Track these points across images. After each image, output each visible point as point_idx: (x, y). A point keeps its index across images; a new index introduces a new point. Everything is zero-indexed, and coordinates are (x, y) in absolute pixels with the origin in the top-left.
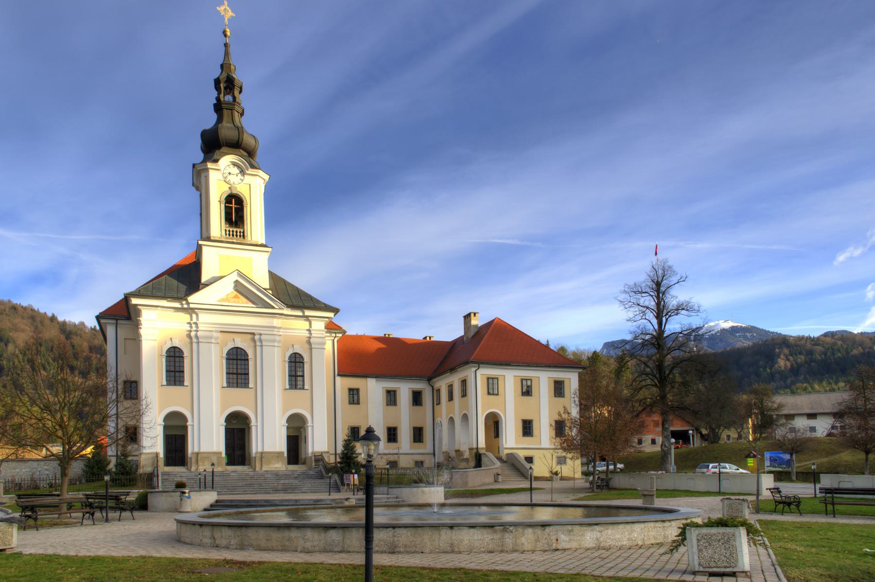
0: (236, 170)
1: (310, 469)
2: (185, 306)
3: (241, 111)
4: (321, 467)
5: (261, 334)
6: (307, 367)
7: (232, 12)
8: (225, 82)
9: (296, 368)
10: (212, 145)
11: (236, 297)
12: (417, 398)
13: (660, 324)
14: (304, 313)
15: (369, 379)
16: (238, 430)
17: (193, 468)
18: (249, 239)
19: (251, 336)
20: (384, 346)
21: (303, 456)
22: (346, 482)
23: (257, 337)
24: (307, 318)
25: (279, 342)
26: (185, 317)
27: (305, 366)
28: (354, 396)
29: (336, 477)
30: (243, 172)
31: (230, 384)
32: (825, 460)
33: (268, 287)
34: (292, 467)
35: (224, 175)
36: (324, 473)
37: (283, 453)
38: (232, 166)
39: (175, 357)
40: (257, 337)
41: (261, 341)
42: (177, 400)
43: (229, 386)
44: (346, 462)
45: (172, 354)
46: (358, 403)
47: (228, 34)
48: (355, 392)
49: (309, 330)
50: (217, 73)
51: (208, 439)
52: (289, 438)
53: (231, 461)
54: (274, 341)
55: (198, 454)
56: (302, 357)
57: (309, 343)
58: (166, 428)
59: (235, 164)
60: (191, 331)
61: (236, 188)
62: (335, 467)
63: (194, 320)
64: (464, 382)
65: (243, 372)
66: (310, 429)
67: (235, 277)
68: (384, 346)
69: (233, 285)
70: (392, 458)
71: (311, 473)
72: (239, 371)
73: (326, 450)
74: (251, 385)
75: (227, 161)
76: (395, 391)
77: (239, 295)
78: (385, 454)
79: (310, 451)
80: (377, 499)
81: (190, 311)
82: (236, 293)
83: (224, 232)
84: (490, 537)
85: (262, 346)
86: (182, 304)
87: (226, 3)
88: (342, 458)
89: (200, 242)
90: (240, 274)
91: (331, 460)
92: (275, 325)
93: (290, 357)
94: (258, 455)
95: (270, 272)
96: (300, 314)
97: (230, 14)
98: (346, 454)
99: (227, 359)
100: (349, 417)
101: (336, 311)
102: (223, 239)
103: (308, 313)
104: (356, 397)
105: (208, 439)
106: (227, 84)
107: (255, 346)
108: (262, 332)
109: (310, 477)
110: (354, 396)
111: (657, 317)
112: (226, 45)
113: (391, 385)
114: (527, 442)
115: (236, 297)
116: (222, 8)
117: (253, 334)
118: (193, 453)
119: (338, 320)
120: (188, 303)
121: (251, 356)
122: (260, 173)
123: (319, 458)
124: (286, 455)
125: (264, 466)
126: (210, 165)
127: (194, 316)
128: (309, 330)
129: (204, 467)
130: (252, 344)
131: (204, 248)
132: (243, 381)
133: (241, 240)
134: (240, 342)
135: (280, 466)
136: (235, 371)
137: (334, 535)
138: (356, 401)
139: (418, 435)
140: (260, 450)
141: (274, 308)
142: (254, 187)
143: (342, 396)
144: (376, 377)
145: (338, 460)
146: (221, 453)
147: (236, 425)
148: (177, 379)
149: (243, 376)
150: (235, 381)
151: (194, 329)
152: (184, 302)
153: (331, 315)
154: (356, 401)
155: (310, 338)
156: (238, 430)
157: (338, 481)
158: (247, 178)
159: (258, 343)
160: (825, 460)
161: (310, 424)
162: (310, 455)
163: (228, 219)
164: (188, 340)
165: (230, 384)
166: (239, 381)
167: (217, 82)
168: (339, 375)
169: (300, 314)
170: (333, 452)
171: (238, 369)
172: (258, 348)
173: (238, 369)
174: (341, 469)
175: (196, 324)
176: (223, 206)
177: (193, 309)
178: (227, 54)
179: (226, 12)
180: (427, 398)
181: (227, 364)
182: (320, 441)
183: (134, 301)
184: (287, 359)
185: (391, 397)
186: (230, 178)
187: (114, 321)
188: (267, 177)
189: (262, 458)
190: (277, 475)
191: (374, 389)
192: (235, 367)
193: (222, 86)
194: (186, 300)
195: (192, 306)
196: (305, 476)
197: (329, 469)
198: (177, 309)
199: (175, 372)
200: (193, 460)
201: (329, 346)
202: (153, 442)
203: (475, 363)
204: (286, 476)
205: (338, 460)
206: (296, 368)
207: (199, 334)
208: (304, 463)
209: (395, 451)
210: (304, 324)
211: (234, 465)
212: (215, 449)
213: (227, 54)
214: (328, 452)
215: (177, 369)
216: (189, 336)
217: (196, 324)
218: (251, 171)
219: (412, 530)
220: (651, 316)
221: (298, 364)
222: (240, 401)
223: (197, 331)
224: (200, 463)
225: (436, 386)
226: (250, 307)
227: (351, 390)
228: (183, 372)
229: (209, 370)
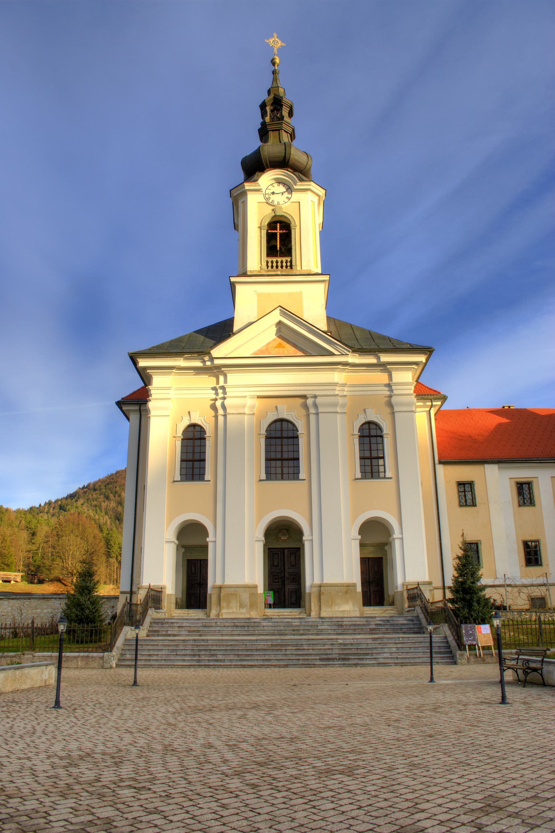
0: (282, 189)
1: (401, 613)
2: (208, 363)
3: (290, 130)
4: (418, 610)
5: (315, 397)
6: (388, 442)
7: (282, 42)
8: (272, 105)
9: (371, 448)
10: (254, 167)
11: (279, 346)
14: (378, 358)
15: (487, 466)
16: (284, 552)
17: (213, 613)
18: (298, 268)
19: (301, 401)
20: (505, 420)
21: (390, 591)
22: (467, 641)
23: (310, 401)
24: (383, 367)
25: (343, 406)
26: (208, 381)
27: (385, 440)
28: (466, 493)
29: (445, 630)
30: (290, 189)
31: (270, 475)
34: (371, 611)
35: (266, 196)
36: (424, 621)
37: (354, 585)
38: (275, 185)
39: (370, 436)
40: (310, 401)
41: (315, 406)
42: (194, 503)
44: (463, 599)
46: (474, 505)
47: (277, 61)
48: (467, 488)
49: (389, 386)
50: (264, 96)
51: (240, 566)
52: (364, 561)
53: (280, 602)
54: (336, 405)
55: (220, 588)
56: (380, 429)
57: (390, 405)
59: (279, 182)
60: (216, 400)
61: (281, 208)
62: (444, 610)
63: (221, 383)
65: (291, 456)
66: (397, 544)
67: (276, 317)
68: (505, 420)
69: (274, 329)
70: (537, 592)
71: (402, 621)
72: (285, 456)
73: (427, 579)
74: (302, 475)
75: (267, 179)
76: (529, 484)
77: (284, 343)
78: (525, 586)
79: (400, 581)
80: (504, 653)
81: (216, 371)
82: (280, 340)
83: (264, 264)
85: (317, 414)
86: (204, 362)
88: (455, 590)
89: (233, 279)
90: (285, 312)
91: (435, 597)
92: (336, 381)
93: (361, 429)
94: (315, 590)
96: (373, 361)
97: (280, 44)
98: (463, 583)
99: (267, 438)
100: (460, 525)
102: (263, 273)
103: (385, 358)
104: (469, 496)
107: (308, 415)
108: (317, 393)
109: (397, 629)
110: (466, 493)
112: (274, 72)
113: (523, 473)
115: (279, 346)
116: (271, 40)
117: (305, 397)
118: (214, 587)
120: (212, 359)
121: (301, 430)
122: (313, 186)
123: (415, 595)
124: (359, 589)
125: (323, 609)
126: (248, 186)
127: (221, 378)
128: (389, 386)
129: (231, 611)
130: (304, 412)
131: (238, 288)
132: (291, 470)
133: (288, 271)
134: (287, 411)
135: (351, 608)
136: (279, 456)
138: (469, 501)
140: (317, 581)
141: (332, 354)
142: (307, 209)
143: (448, 495)
144: (498, 462)
145: (449, 595)
146: (256, 587)
147: (284, 542)
148: (196, 471)
149: (291, 463)
150: (279, 470)
151: (221, 395)
152: (206, 358)
154: (469, 501)
155: (390, 396)
156: (284, 552)
157: (451, 639)
158: (296, 196)
159: (312, 411)
161: (396, 534)
162: (400, 589)
163: (271, 251)
164: (213, 413)
165: (270, 475)
166: (285, 470)
167: (263, 106)
168: (440, 463)
169: (373, 361)
170: (440, 584)
172: (313, 418)
173: (282, 448)
174: (456, 612)
175: (223, 388)
176: (264, 232)
177: (219, 367)
178: (275, 80)
179: (275, 43)
181: (268, 446)
182: (416, 566)
184: (356, 432)
186: (273, 197)
187: (137, 408)
188: (321, 192)
189: (320, 594)
190: (340, 626)
191: (496, 482)
192: (279, 448)
193: (268, 109)
194: (209, 353)
195: (217, 362)
196: (390, 626)
197: (434, 616)
198: (198, 370)
199: (193, 461)
200: (214, 599)
201: (421, 423)
204: (355, 628)
205: (449, 595)
206: (371, 448)
207: (227, 402)
208: (392, 604)
209: (541, 581)
210: (381, 377)
211: (284, 606)
212: (247, 581)
213: (275, 80)
214: (430, 583)
215: (197, 457)
216: (214, 407)
217: (223, 388)
218: (300, 185)
221: (373, 440)
222: (286, 502)
223: (224, 398)
224: (223, 604)
226: (300, 354)
228: (204, 460)
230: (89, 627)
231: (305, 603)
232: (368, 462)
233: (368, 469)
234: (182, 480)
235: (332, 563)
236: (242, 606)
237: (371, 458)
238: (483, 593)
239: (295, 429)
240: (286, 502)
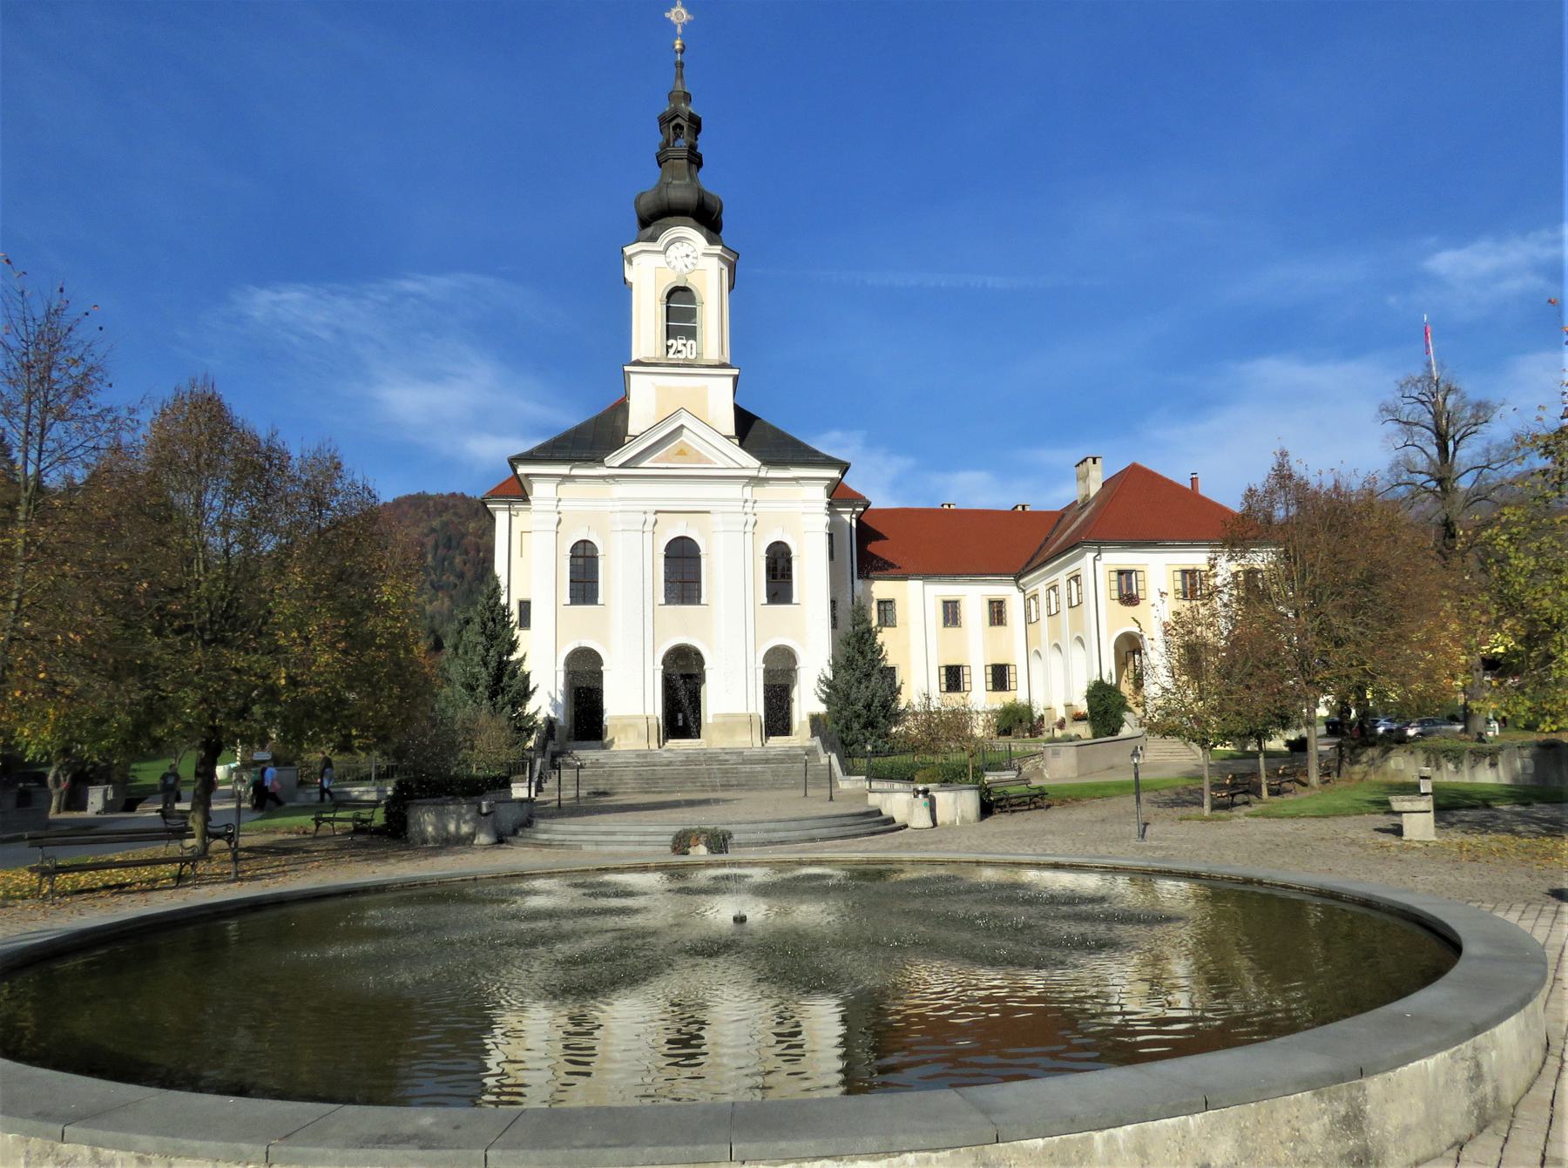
12: (997, 612)
16: (683, 679)
32: (992, 980)
45: (580, 552)
51: (631, 699)
58: (767, 672)
84: (550, 1014)
87: (679, 3)
89: (627, 368)
95: (737, 408)
101: (844, 468)
105: (631, 699)
113: (950, 590)
114: (954, 700)
119: (853, 482)
153: (835, 474)
156: (683, 679)
160: (992, 980)
171: (683, 570)
173: (683, 570)
179: (678, 15)
183: (522, 470)
185: (951, 612)
202: (546, 698)
203: (1093, 544)
222: (682, 625)
229: (632, 571)
239: (594, 548)
240: (682, 625)
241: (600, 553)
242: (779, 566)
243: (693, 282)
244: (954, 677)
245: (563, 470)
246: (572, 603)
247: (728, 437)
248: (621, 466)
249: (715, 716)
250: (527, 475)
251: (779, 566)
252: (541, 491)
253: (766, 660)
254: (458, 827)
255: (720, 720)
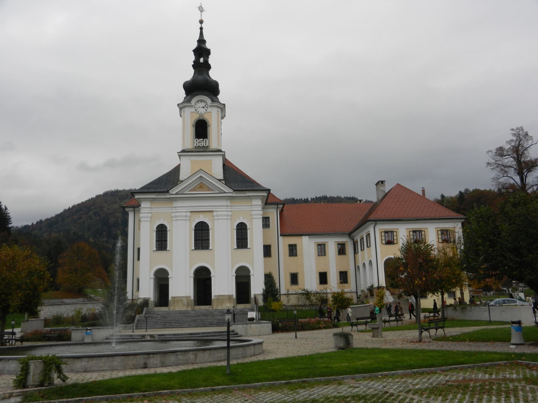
12: (342, 250)
13: (522, 179)
15: (303, 237)
16: (202, 279)
33: (222, 178)
39: (242, 229)
43: (196, 249)
45: (160, 229)
50: (195, 45)
51: (182, 287)
64: (368, 235)
76: (324, 245)
106: (202, 51)
111: (519, 174)
113: (321, 240)
137: (191, 356)
139: (343, 277)
144: (309, 235)
148: (163, 246)
149: (198, 238)
156: (202, 279)
166: (203, 245)
168: (281, 235)
171: (202, 236)
173: (202, 236)
180: (349, 248)
185: (322, 250)
202: (147, 291)
219: (123, 358)
220: (512, 172)
222: (202, 259)
225: (355, 239)
227: (290, 246)
229: (181, 236)
230: (369, 295)
231: (116, 379)
232: (240, 241)
233: (240, 244)
234: (156, 250)
235: (223, 286)
236: (184, 305)
237: (242, 239)
238: (346, 295)
239: (208, 226)
240: (202, 259)
241: (248, 227)
242: (242, 231)
243: (206, 117)
244: (323, 278)
245: (153, 196)
246: (196, 249)
247: (219, 180)
248: (176, 194)
249: (215, 296)
250: (139, 198)
251: (242, 231)
252: (145, 205)
253: (236, 272)
254: (492, 272)
255: (216, 297)
